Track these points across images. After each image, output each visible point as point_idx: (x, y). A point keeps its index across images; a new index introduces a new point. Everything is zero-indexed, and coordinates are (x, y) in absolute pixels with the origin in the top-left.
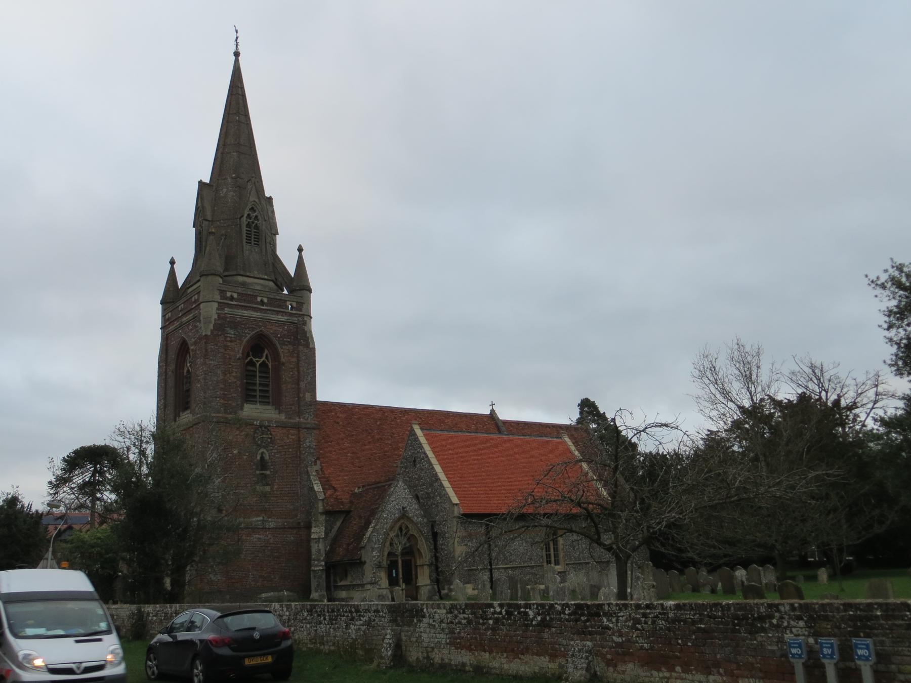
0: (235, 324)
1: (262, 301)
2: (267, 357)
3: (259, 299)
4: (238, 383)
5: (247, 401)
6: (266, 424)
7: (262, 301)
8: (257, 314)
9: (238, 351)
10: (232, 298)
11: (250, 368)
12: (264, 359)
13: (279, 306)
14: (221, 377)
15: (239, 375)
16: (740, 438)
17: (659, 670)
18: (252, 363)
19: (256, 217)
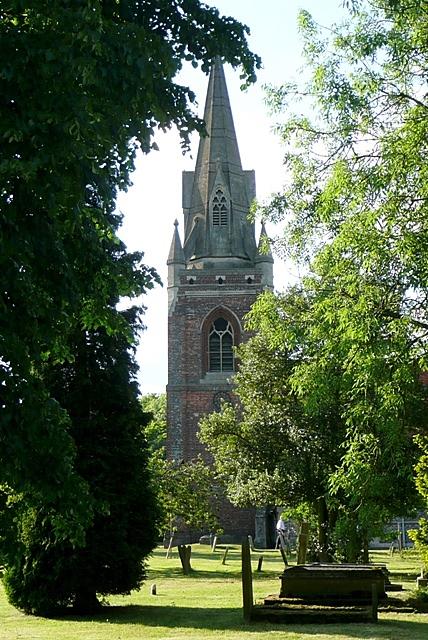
0: (195, 303)
1: (220, 279)
2: (230, 329)
3: (217, 278)
4: (199, 355)
5: (211, 370)
6: (225, 389)
7: (220, 279)
8: (217, 292)
9: (199, 326)
10: (220, 281)
11: (214, 340)
12: (227, 330)
13: (237, 281)
14: (182, 352)
15: (200, 348)
16: (81, 307)
17: (344, 451)
18: (215, 336)
19: (223, 198)
